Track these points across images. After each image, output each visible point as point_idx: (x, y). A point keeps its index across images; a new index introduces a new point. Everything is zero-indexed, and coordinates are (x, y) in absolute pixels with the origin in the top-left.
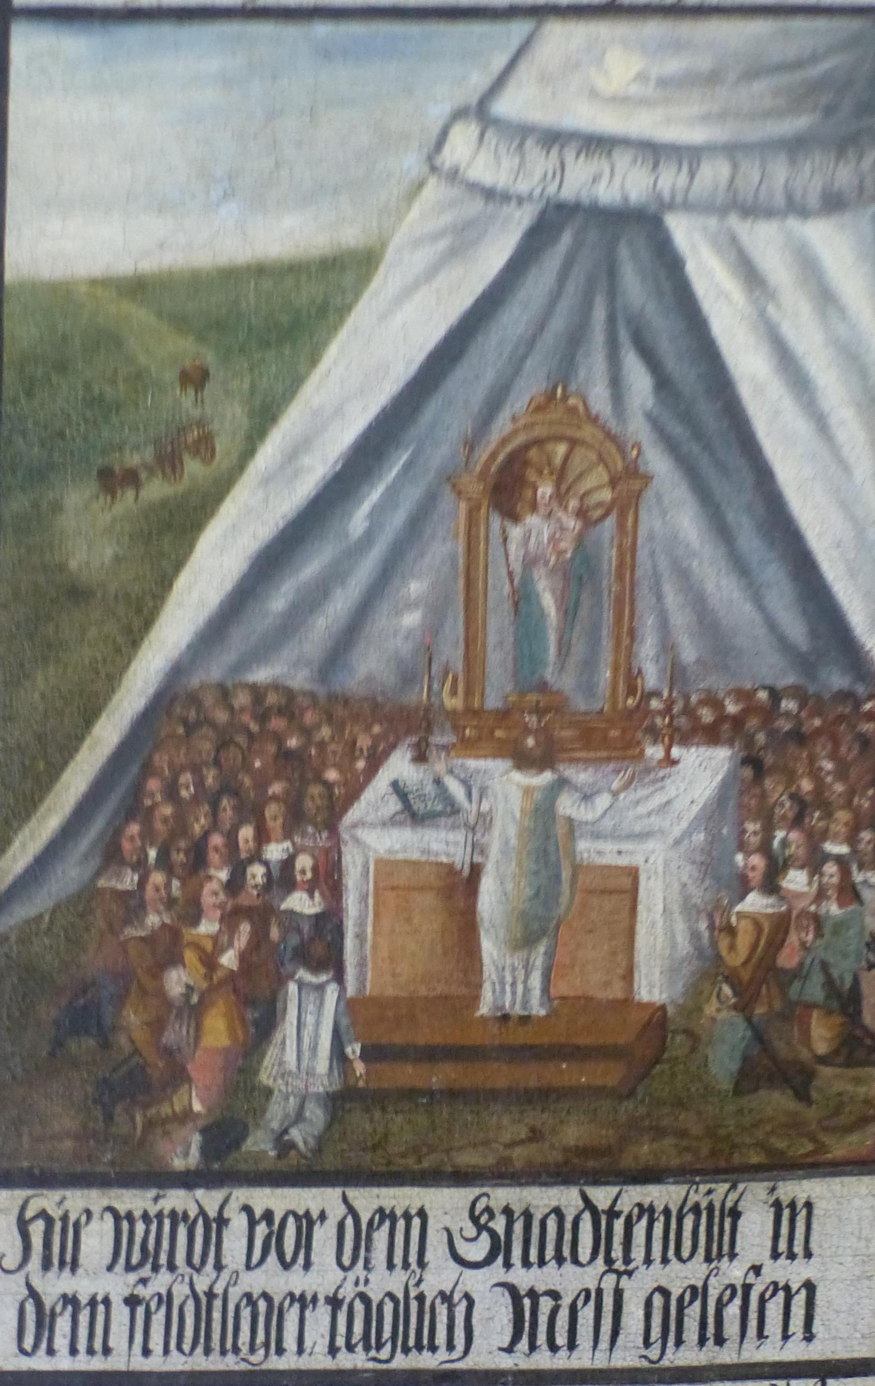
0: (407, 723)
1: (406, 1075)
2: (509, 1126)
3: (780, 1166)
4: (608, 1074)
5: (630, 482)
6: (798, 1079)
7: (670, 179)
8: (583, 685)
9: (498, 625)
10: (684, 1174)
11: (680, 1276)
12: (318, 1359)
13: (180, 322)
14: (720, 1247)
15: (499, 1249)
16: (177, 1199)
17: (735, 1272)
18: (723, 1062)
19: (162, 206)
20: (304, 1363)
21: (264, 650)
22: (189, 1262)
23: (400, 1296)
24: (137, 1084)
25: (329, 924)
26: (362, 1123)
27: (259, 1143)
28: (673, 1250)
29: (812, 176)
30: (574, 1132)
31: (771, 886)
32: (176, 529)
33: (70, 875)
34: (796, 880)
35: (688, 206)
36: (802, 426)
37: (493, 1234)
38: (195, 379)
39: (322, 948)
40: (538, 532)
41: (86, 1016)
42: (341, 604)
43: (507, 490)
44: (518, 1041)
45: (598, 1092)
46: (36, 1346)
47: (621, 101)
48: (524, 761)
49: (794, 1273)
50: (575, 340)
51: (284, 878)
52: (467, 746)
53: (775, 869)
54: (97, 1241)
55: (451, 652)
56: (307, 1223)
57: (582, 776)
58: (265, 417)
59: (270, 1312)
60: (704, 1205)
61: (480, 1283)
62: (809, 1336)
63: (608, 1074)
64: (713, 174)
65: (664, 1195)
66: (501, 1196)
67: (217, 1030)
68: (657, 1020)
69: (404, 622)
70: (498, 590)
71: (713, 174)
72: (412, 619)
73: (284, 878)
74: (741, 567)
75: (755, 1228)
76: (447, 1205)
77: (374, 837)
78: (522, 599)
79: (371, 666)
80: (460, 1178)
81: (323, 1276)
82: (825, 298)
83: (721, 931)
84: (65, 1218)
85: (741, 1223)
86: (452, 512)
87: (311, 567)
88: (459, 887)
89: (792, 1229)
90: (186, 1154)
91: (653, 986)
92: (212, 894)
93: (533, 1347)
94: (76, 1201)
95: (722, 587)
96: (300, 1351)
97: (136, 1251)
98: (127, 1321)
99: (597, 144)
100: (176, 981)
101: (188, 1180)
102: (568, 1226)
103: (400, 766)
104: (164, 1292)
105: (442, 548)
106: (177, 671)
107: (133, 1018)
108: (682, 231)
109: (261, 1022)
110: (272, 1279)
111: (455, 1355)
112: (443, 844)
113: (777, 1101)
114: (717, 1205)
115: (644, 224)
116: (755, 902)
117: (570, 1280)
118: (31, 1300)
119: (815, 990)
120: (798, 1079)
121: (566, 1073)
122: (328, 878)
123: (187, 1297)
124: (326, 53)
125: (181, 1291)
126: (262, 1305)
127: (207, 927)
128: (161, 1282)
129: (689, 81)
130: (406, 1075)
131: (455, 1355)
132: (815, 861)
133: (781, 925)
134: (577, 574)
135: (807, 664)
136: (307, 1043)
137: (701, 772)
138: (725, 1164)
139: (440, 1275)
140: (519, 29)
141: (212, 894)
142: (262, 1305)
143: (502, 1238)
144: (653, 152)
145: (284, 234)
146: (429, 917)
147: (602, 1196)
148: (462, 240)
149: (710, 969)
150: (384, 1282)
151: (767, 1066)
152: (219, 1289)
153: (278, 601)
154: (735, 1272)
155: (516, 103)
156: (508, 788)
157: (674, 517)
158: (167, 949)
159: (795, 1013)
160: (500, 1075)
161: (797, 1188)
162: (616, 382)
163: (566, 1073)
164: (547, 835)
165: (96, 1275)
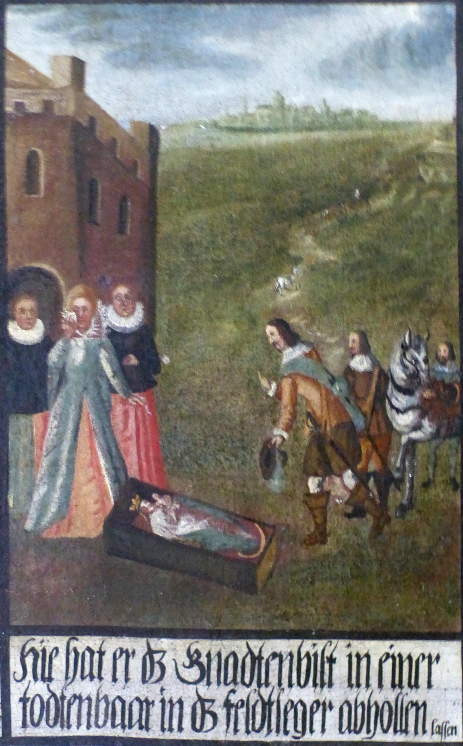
12: (332, 735)
20: (327, 737)
22: (299, 684)
23: (353, 703)
37: (200, 665)
46: (105, 722)
60: (311, 653)
62: (323, 730)
84: (44, 651)
85: (334, 666)
93: (269, 731)
96: (323, 730)
98: (21, 711)
102: (223, 661)
104: (245, 699)
111: (370, 735)
114: (319, 653)
118: (53, 698)
123: (257, 701)
125: (254, 698)
126: (300, 708)
128: (242, 693)
131: (370, 735)
142: (300, 708)
143: (206, 668)
152: (274, 698)
161: (360, 646)
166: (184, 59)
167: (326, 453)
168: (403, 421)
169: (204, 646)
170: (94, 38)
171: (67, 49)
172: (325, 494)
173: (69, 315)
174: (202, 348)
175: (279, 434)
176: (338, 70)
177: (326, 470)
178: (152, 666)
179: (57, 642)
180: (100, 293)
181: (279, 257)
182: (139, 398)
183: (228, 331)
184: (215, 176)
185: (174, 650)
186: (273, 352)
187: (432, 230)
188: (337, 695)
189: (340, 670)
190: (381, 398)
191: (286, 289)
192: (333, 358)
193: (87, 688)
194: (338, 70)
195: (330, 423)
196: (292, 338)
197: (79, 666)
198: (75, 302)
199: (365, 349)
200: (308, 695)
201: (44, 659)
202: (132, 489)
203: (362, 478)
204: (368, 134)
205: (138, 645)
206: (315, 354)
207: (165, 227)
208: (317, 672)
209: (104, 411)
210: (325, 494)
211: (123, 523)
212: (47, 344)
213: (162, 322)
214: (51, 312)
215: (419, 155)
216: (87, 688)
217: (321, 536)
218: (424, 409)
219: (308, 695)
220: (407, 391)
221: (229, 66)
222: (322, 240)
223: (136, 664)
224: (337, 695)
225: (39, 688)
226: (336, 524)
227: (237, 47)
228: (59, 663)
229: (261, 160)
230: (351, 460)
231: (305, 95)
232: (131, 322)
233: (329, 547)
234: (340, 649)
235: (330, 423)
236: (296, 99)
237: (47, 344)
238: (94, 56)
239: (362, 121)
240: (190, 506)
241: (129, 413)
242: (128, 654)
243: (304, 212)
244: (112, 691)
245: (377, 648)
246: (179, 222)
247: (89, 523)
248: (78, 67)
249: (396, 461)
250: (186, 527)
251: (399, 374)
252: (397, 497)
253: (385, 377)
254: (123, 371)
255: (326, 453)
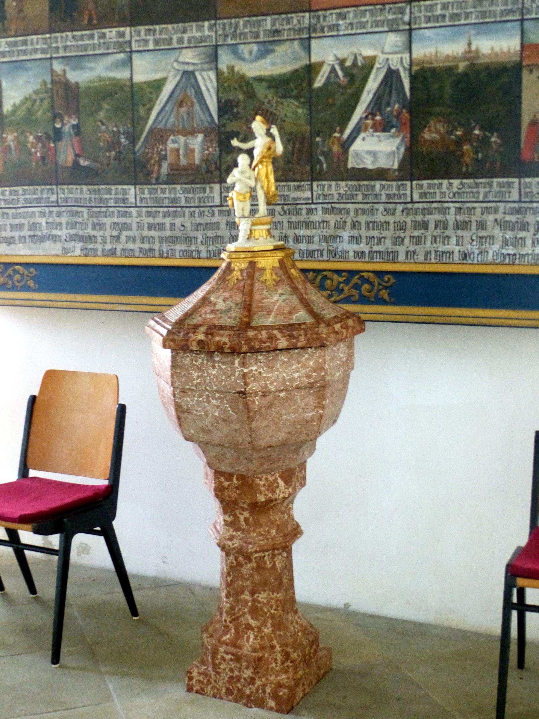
0: (173, 132)
1: (174, 172)
2: (183, 178)
3: (210, 183)
4: (192, 172)
5: (192, 103)
6: (211, 172)
7: (195, 67)
8: (189, 128)
9: (180, 120)
10: (201, 183)
11: (201, 195)
13: (149, 87)
14: (205, 192)
15: (183, 192)
16: (154, 186)
17: (206, 195)
18: (204, 171)
19: (147, 73)
21: (159, 124)
24: (149, 173)
25: (166, 155)
26: (170, 178)
27: (160, 180)
28: (200, 192)
29: (206, 66)
30: (190, 179)
31: (208, 150)
32: (150, 110)
33: (142, 150)
34: (210, 149)
35: (197, 70)
36: (209, 96)
38: (151, 93)
39: (165, 158)
40: (184, 110)
41: (144, 166)
42: (166, 118)
43: (181, 105)
44: (185, 168)
45: (192, 174)
47: (190, 58)
48: (184, 136)
49: (212, 195)
50: (186, 87)
51: (162, 150)
52: (178, 134)
53: (208, 148)
54: (146, 191)
55: (176, 124)
56: (165, 189)
57: (189, 137)
58: (158, 97)
59: (162, 199)
61: (182, 196)
63: (192, 172)
64: (199, 66)
65: (198, 186)
66: (184, 186)
67: (156, 167)
68: (197, 166)
69: (172, 120)
70: (180, 116)
71: (199, 66)
72: (172, 120)
73: (162, 150)
74: (204, 113)
75: (208, 190)
76: (178, 187)
77: (170, 145)
78: (183, 117)
79: (169, 125)
80: (180, 184)
81: (167, 195)
82: (211, 81)
83: (240, 218)
86: (176, 107)
87: (163, 114)
88: (178, 150)
89: (211, 191)
90: (154, 181)
91: (197, 162)
92: (155, 152)
94: (144, 187)
95: (201, 114)
97: (150, 193)
99: (188, 64)
100: (152, 162)
101: (154, 184)
103: (172, 137)
105: (175, 112)
106: (151, 126)
107: (149, 166)
108: (197, 74)
109: (160, 166)
110: (163, 196)
112: (176, 146)
113: (209, 175)
115: (192, 73)
116: (206, 152)
117: (190, 196)
119: (212, 162)
120: (211, 172)
121: (189, 172)
122: (166, 150)
124: (163, 54)
127: (155, 156)
129: (198, 55)
130: (174, 172)
132: (212, 147)
133: (209, 155)
134: (188, 114)
135: (210, 124)
136: (165, 168)
137: (200, 137)
138: (205, 183)
139: (178, 195)
140: (180, 50)
141: (155, 152)
144: (194, 64)
145: (158, 76)
146: (175, 153)
147: (193, 186)
148: (175, 76)
149: (202, 159)
150: (173, 196)
151: (209, 171)
153: (160, 118)
154: (206, 195)
155: (181, 59)
156: (182, 139)
157: (197, 107)
158: (151, 158)
159: (210, 164)
160: (182, 172)
162: (191, 92)
163: (189, 172)
164: (186, 144)
165: (146, 195)
166: (83, 68)
167: (110, 148)
168: (123, 140)
169: (90, 187)
170: (67, 65)
171: (63, 68)
172: (109, 156)
173: (65, 122)
174: (88, 127)
175: (101, 144)
176: (108, 69)
177: (109, 151)
178: (82, 191)
179: (65, 187)
180: (70, 117)
181: (99, 108)
182: (77, 138)
183: (92, 124)
184: (101, 113)
185: (85, 187)
186: (99, 127)
187: (133, 111)
188: (113, 196)
189: (113, 192)
190: (119, 137)
191: (102, 114)
192: (110, 128)
193: (71, 196)
194: (108, 69)
195: (110, 141)
196: (103, 124)
197: (70, 192)
198: (66, 119)
199: (116, 126)
200: (107, 196)
201: (63, 190)
202: (77, 156)
203: (116, 152)
204: (115, 82)
205: (78, 187)
206: (107, 128)
207: (81, 102)
208: (109, 192)
209: (71, 140)
210: (109, 156)
211: (76, 163)
212: (62, 128)
213: (81, 123)
214: (62, 120)
215: (124, 85)
216: (71, 196)
217: (109, 164)
218: (126, 138)
219: (107, 196)
220: (123, 134)
221: (91, 69)
222: (108, 104)
223: (79, 191)
224: (113, 196)
225: (63, 196)
226: (112, 162)
227: (92, 65)
228: (66, 191)
229: (96, 88)
230: (114, 149)
231: (105, 74)
232: (75, 122)
233: (111, 167)
234: (113, 187)
235: (110, 141)
236: (103, 75)
237: (62, 128)
238: (67, 68)
239: (113, 79)
240: (87, 159)
241: (76, 140)
242: (77, 189)
243: (103, 99)
244: (75, 196)
245: (119, 187)
246: (84, 102)
247: (70, 164)
248: (65, 71)
249: (122, 148)
250: (86, 163)
251: (122, 131)
252: (122, 156)
253: (119, 132)
254: (75, 133)
255: (110, 148)
